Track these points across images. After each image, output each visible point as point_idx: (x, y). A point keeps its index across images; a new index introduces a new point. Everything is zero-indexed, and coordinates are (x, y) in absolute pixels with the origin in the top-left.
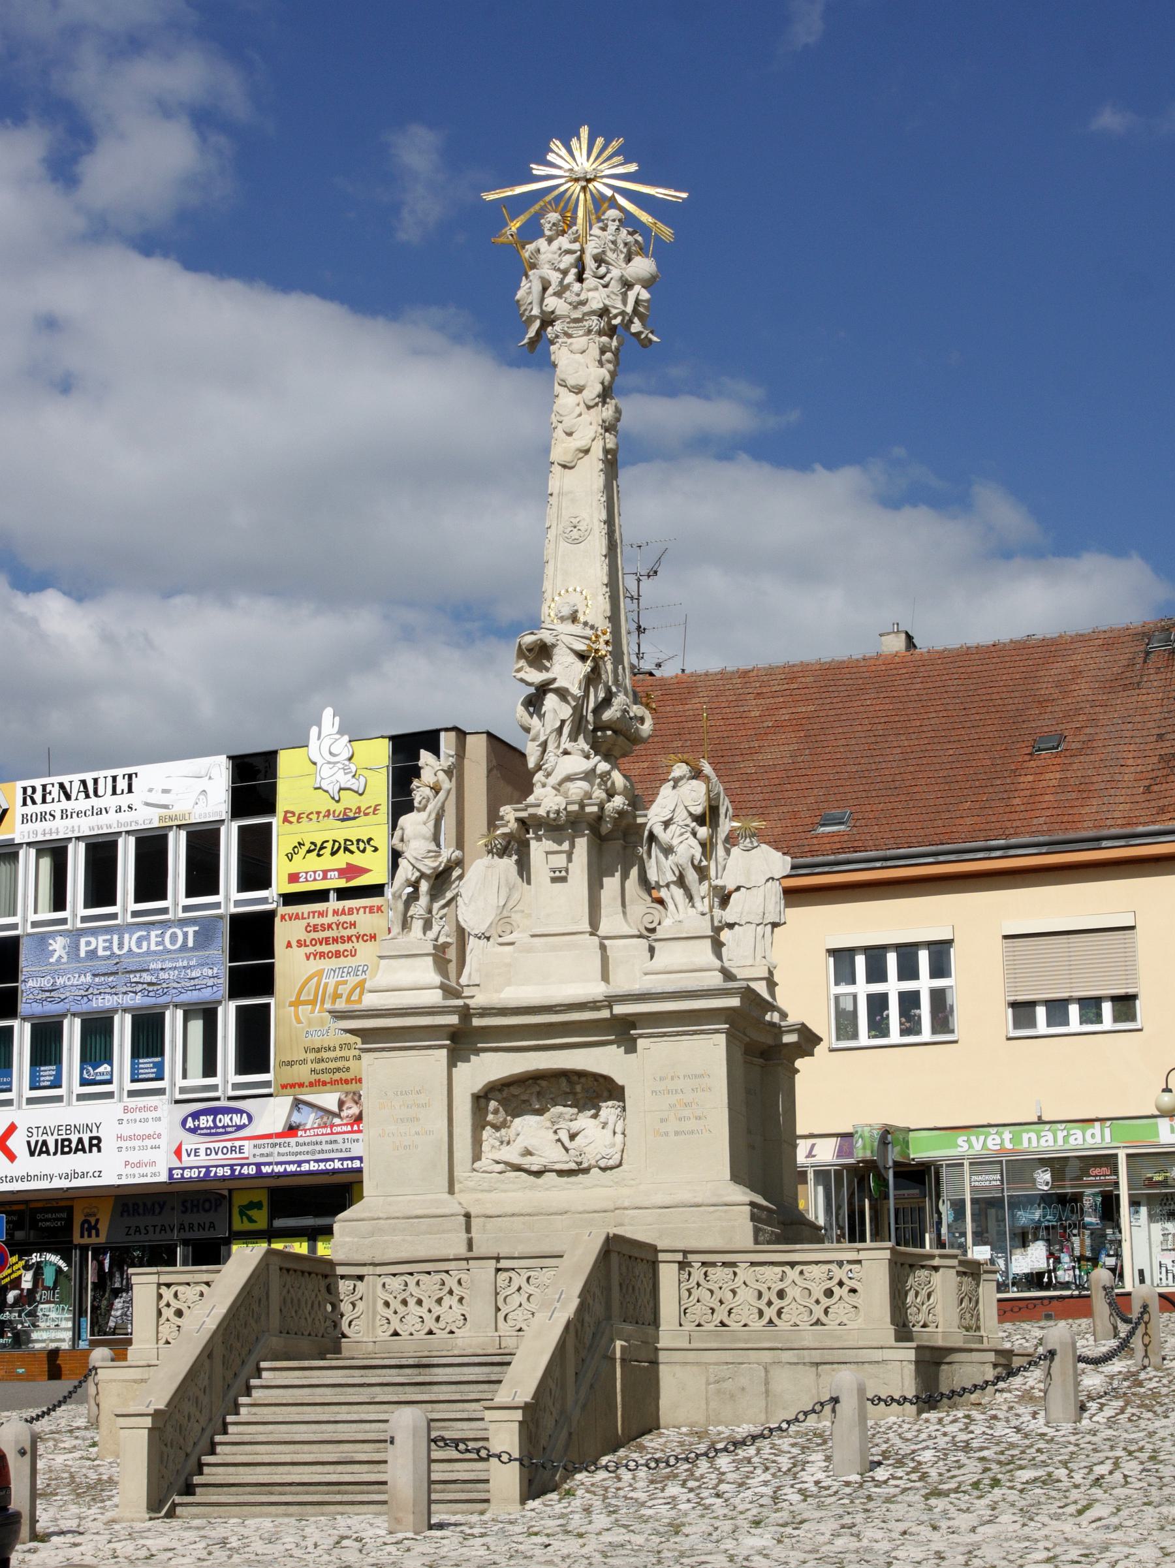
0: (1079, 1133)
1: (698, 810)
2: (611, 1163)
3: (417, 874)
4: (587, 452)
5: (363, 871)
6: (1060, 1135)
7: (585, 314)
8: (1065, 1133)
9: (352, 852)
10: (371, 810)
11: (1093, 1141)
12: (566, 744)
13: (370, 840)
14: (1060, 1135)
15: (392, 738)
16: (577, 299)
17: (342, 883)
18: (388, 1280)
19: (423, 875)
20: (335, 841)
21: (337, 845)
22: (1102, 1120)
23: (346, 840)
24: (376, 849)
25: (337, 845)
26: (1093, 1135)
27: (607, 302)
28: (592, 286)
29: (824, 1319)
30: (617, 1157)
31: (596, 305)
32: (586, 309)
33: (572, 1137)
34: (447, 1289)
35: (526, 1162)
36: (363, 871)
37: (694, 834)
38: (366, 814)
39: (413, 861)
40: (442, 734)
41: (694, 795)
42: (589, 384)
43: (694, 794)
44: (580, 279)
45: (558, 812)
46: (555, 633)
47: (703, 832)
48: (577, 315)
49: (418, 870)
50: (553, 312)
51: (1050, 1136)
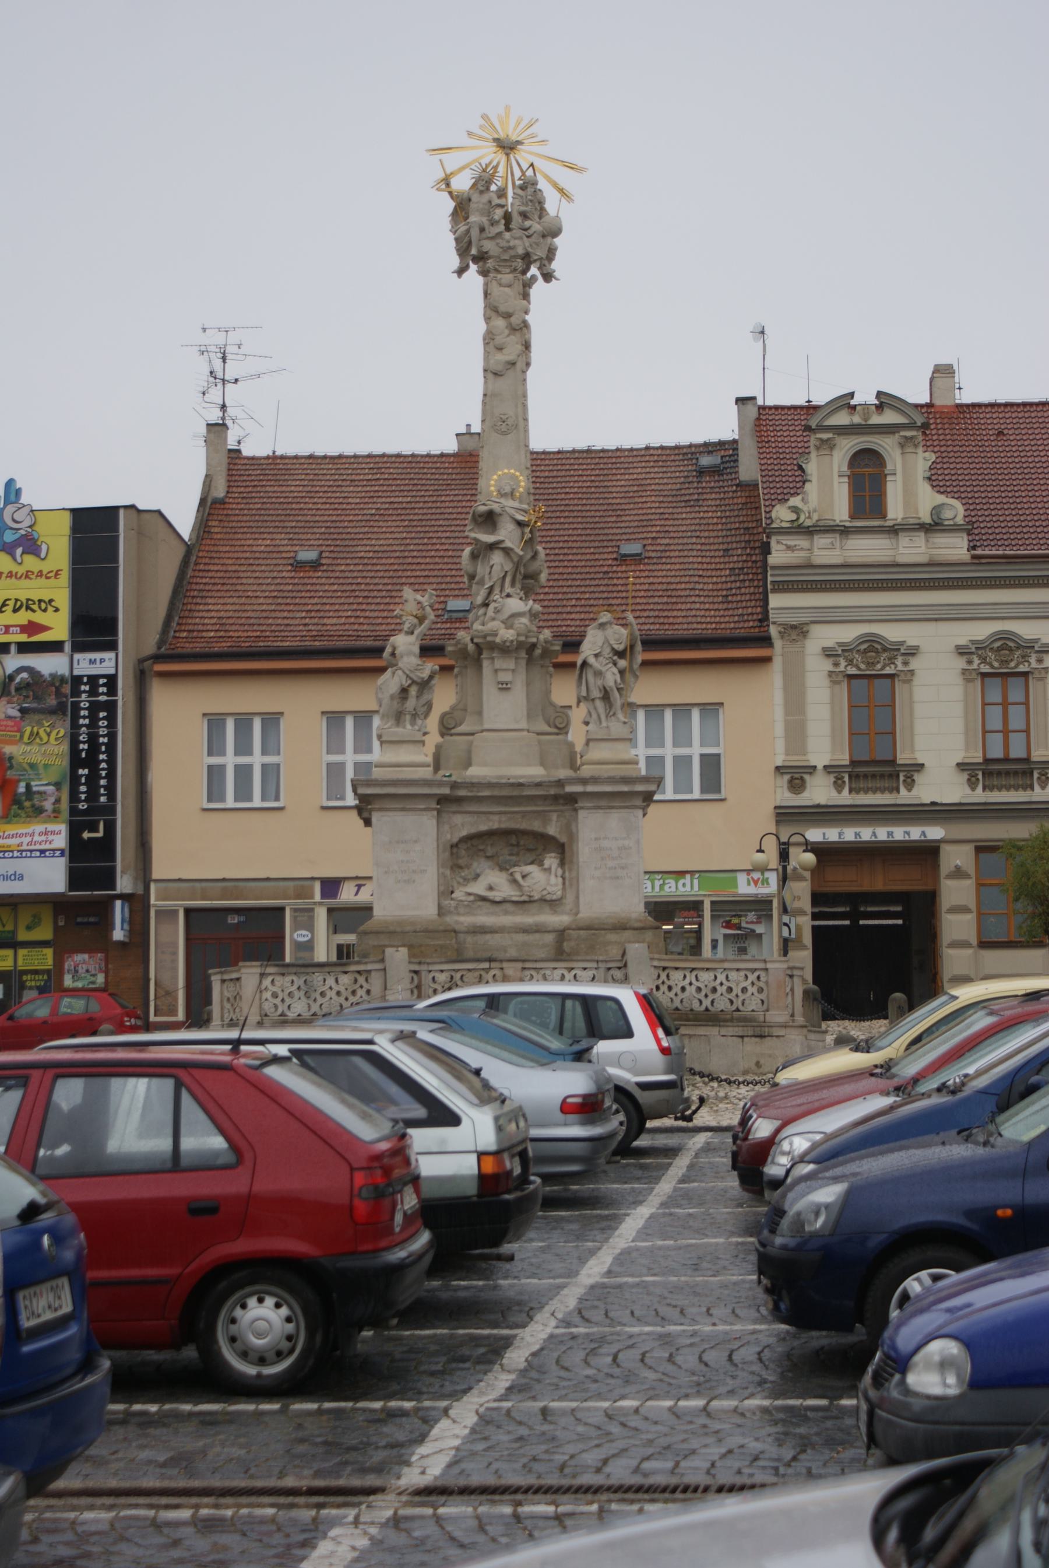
0: (673, 883)
1: (620, 647)
2: (554, 897)
3: (409, 682)
4: (514, 364)
5: (44, 628)
6: (657, 883)
7: (512, 257)
8: (661, 882)
9: (33, 611)
10: (52, 574)
11: (683, 890)
13: (51, 601)
14: (657, 883)
15: (75, 511)
17: (23, 638)
18: (438, 975)
19: (414, 682)
20: (17, 600)
21: (19, 603)
22: (692, 873)
23: (28, 600)
24: (57, 610)
25: (19, 603)
26: (684, 885)
27: (530, 250)
28: (517, 235)
29: (741, 1008)
30: (559, 893)
31: (520, 251)
33: (524, 877)
34: (358, 985)
35: (490, 895)
36: (44, 628)
37: (615, 664)
38: (47, 578)
39: (408, 672)
40: (122, 512)
44: (508, 229)
45: (512, 641)
47: (623, 663)
50: (486, 253)
51: (649, 884)
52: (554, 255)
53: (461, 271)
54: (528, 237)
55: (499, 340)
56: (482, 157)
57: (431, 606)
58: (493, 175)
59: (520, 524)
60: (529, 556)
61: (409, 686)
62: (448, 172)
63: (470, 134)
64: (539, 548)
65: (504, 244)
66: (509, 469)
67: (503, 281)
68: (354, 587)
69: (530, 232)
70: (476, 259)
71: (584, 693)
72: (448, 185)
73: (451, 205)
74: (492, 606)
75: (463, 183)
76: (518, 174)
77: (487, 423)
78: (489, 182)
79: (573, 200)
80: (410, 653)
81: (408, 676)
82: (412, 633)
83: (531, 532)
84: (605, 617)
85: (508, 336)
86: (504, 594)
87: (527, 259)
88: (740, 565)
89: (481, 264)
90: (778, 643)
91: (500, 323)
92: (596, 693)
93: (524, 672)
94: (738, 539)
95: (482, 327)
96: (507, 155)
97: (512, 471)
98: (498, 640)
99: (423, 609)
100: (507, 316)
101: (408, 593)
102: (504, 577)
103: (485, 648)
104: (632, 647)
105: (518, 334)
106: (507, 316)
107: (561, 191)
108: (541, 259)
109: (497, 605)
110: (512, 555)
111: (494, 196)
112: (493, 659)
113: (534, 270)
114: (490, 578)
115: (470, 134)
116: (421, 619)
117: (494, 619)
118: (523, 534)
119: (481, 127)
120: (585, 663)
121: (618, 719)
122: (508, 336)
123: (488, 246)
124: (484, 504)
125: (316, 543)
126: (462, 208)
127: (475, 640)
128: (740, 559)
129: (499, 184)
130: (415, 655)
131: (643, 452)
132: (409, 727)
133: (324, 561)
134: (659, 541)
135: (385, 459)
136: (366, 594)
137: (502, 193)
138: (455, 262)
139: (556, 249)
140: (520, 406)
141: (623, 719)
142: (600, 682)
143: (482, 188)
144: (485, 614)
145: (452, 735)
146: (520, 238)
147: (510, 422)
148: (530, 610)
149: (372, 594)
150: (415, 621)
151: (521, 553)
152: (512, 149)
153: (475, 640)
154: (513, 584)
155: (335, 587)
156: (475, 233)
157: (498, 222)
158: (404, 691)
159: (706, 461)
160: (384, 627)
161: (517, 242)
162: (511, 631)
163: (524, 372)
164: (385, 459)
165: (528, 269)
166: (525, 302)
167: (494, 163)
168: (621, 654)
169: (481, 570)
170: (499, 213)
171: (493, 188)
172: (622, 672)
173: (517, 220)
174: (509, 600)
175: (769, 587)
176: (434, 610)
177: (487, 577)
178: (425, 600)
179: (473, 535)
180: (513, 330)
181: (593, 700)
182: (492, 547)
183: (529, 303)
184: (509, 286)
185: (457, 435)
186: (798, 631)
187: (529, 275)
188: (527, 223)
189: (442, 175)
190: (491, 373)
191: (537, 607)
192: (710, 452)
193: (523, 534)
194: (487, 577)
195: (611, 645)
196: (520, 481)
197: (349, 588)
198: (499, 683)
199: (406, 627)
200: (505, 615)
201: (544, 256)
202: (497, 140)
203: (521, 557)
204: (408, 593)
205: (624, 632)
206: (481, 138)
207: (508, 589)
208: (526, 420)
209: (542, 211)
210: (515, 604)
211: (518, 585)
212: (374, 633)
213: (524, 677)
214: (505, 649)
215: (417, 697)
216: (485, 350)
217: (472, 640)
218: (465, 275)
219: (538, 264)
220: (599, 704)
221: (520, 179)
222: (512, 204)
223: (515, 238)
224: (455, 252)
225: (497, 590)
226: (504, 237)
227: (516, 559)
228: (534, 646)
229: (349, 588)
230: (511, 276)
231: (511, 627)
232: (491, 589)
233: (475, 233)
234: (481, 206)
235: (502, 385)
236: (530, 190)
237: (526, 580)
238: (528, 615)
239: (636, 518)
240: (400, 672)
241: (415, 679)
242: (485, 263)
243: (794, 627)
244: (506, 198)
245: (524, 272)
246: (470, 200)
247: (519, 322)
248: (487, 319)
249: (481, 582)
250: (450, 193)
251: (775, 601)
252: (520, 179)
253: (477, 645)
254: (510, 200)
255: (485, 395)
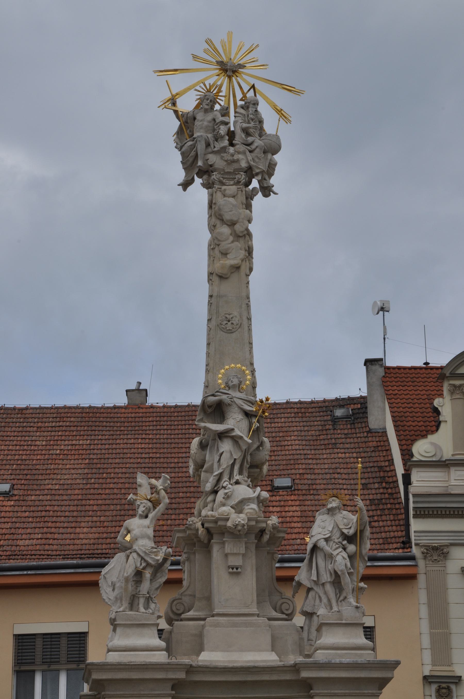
3: (144, 564)
7: (235, 170)
12: (237, 477)
16: (230, 158)
27: (252, 163)
28: (241, 150)
31: (244, 164)
32: (235, 166)
37: (345, 549)
39: (142, 555)
41: (348, 521)
42: (241, 220)
43: (345, 520)
45: (243, 525)
46: (230, 396)
47: (352, 548)
48: (230, 169)
49: (145, 561)
50: (211, 166)
52: (274, 170)
53: (186, 185)
54: (250, 152)
55: (224, 245)
56: (206, 79)
57: (165, 490)
58: (217, 95)
59: (247, 414)
60: (255, 446)
61: (144, 568)
62: (174, 93)
63: (195, 57)
64: (266, 440)
65: (227, 157)
66: (236, 363)
67: (228, 192)
68: (43, 514)
69: (253, 147)
70: (200, 174)
71: (314, 578)
72: (174, 104)
73: (176, 124)
74: (221, 494)
75: (187, 104)
76: (239, 95)
77: (214, 322)
78: (214, 102)
79: (290, 121)
80: (144, 536)
81: (142, 558)
82: (146, 517)
83: (258, 421)
84: (334, 503)
85: (232, 242)
86: (233, 481)
87: (250, 172)
88: (379, 496)
89: (205, 177)
90: (421, 563)
91: (226, 230)
92: (326, 577)
93: (254, 557)
94: (374, 476)
95: (207, 236)
96: (230, 77)
97: (239, 365)
98: (229, 524)
99: (158, 493)
100: (232, 224)
101: (141, 479)
102: (233, 465)
103: (217, 530)
104: (362, 532)
105: (242, 240)
106: (232, 224)
107: (279, 112)
108: (262, 172)
109: (226, 491)
110: (240, 442)
111: (219, 115)
112: (224, 543)
113: (255, 183)
114: (219, 466)
115: (195, 57)
116: (155, 503)
117: (224, 505)
118: (251, 424)
119: (205, 51)
120: (315, 548)
121: (350, 604)
122: (232, 242)
123: (213, 159)
124: (213, 395)
125: (9, 477)
126: (187, 123)
127: (206, 525)
128: (377, 491)
129: (222, 103)
130: (149, 538)
131: (284, 406)
132: (142, 609)
133: (16, 492)
134: (306, 476)
135: (66, 410)
136: (54, 519)
137: (225, 112)
138: (181, 175)
139: (275, 165)
140: (244, 306)
141: (355, 604)
142: (330, 567)
143: (206, 107)
144: (214, 501)
145: (181, 620)
146: (244, 153)
147: (235, 321)
148: (258, 497)
149: (59, 519)
150: (150, 504)
151: (250, 441)
152: (234, 72)
153: (206, 525)
154: (240, 473)
155: (27, 514)
156: (201, 147)
157: (222, 137)
158: (139, 574)
159: (339, 413)
160: (71, 547)
161: (241, 156)
162: (242, 516)
163: (248, 275)
164: (66, 410)
165: (250, 183)
166: (248, 211)
167: (219, 83)
168: (350, 539)
169: (210, 457)
170: (223, 130)
171: (217, 107)
172: (351, 557)
173: (240, 137)
174: (237, 486)
175: (411, 512)
176: (167, 493)
177: (216, 465)
178: (159, 484)
179: (203, 424)
180: (237, 237)
181: (323, 584)
182: (222, 435)
183: (251, 212)
184: (234, 197)
185: (127, 391)
186: (438, 553)
187: (251, 187)
188: (250, 139)
189: (169, 96)
190: (217, 276)
191: (265, 494)
192: (341, 406)
193: (251, 424)
194: (216, 465)
195: (340, 530)
196: (246, 375)
197: (39, 514)
198: (229, 567)
199: (141, 510)
200: (233, 502)
201: (266, 170)
202: (220, 63)
203: (249, 446)
204: (141, 479)
205: (354, 518)
206: (206, 61)
207: (237, 477)
208: (249, 319)
209: (262, 133)
210: (243, 491)
211: (246, 473)
212: (63, 553)
213: (254, 561)
214: (235, 533)
215: (151, 580)
216: (209, 255)
217: (203, 525)
218: (190, 188)
219: (259, 177)
220: (328, 587)
221: (241, 100)
222: (235, 122)
223: (239, 153)
224: (181, 166)
225: (226, 478)
226: (225, 153)
227: (244, 447)
228: (262, 532)
229: (39, 514)
230: (234, 187)
231: (240, 512)
232: (220, 476)
233: (201, 147)
234: (206, 123)
235: (226, 288)
236: (251, 110)
237: (252, 469)
238: (256, 501)
239: (284, 457)
240: (135, 555)
241: (150, 561)
242: (210, 176)
243: (435, 549)
244: (229, 117)
245: (248, 184)
246: (195, 119)
247: (242, 229)
248: (212, 228)
249: (210, 471)
250: (176, 112)
251: (416, 525)
252: (241, 100)
253: (208, 530)
254: (232, 119)
255: (211, 296)
